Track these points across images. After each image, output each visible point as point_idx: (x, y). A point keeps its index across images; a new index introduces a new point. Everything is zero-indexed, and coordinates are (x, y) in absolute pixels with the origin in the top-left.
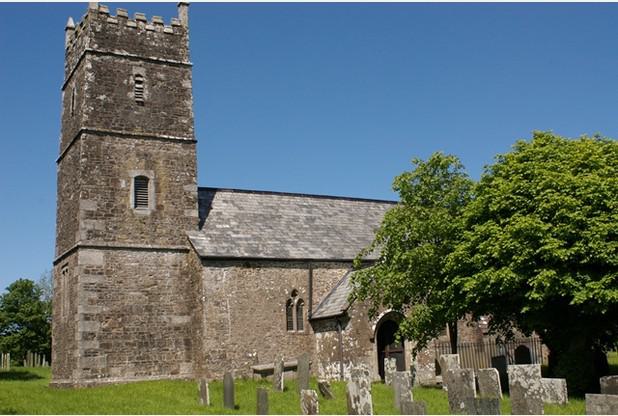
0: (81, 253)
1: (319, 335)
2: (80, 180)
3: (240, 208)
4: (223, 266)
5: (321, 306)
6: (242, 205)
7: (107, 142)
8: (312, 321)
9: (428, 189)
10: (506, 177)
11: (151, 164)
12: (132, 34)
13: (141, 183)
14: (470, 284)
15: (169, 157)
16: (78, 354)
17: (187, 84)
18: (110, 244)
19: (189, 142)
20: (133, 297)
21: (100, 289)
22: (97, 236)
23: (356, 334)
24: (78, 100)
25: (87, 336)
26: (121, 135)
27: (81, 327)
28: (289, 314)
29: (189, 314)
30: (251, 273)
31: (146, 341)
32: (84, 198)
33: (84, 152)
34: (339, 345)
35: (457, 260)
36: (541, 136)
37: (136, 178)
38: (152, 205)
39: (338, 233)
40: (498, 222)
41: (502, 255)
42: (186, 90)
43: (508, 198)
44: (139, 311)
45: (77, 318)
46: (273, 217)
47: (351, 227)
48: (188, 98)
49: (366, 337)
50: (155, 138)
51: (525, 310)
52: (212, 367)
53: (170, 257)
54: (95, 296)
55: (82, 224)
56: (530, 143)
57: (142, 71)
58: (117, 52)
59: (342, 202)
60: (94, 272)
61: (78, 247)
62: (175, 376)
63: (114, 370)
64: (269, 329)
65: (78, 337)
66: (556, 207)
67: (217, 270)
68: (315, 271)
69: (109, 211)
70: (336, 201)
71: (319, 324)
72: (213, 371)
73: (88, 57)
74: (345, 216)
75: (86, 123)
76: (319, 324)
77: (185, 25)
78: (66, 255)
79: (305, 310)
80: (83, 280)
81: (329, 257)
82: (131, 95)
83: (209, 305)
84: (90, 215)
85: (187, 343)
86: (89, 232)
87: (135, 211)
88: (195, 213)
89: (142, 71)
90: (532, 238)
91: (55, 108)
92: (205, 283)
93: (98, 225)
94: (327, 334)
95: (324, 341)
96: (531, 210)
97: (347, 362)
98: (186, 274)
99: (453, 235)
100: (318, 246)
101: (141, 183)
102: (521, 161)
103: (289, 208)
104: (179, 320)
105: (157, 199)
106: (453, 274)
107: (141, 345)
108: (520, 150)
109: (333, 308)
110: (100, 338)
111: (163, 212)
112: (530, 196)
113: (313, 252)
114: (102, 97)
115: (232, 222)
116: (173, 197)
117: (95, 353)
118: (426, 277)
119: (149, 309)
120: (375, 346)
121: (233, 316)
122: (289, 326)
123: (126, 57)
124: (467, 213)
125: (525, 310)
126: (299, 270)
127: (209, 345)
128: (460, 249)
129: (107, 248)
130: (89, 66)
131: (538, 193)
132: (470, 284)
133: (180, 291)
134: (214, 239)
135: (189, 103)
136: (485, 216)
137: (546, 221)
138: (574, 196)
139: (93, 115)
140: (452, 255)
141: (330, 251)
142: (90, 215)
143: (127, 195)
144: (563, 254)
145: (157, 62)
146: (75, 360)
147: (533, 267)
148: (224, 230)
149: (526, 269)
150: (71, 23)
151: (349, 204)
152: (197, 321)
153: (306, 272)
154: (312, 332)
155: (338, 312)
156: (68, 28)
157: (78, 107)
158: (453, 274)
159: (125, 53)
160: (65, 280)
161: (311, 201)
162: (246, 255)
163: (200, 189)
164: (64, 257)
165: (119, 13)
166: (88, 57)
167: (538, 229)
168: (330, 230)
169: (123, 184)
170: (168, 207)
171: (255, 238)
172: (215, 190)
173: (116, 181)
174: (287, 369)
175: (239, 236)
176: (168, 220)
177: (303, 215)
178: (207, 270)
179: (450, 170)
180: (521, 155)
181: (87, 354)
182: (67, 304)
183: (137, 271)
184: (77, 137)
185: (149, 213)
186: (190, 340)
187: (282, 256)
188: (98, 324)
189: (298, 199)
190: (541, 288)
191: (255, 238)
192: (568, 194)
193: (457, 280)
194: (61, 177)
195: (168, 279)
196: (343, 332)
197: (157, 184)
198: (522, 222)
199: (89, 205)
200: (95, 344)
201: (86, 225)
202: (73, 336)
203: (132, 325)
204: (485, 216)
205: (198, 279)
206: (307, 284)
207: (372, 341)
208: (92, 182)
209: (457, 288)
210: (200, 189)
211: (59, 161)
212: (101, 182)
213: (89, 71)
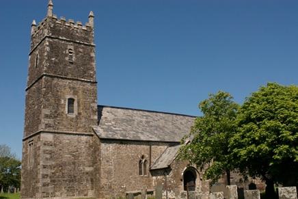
0: (42, 135)
1: (154, 178)
2: (42, 99)
3: (115, 116)
4: (111, 143)
5: (155, 163)
6: (116, 114)
7: (55, 80)
8: (151, 171)
9: (217, 108)
10: (258, 103)
11: (75, 93)
12: (67, 29)
13: (71, 101)
14: (243, 152)
15: (85, 89)
16: (40, 185)
17: (93, 55)
18: (56, 131)
19: (93, 83)
20: (67, 157)
21: (51, 153)
22: (50, 127)
23: (175, 177)
24: (40, 60)
25: (44, 176)
26: (62, 78)
27: (42, 172)
28: (140, 167)
29: (93, 166)
30: (123, 147)
31: (72, 179)
32: (44, 108)
33: (40, 86)
34: (165, 182)
35: (235, 141)
36: (272, 85)
37: (69, 99)
38: (76, 113)
39: (161, 129)
40: (256, 123)
41: (260, 138)
42: (92, 57)
43: (260, 112)
44: (69, 165)
45: (39, 167)
46: (130, 121)
47: (166, 126)
48: (93, 61)
49: (178, 178)
50: (78, 80)
51: (271, 164)
52: (105, 192)
53: (84, 138)
54: (48, 156)
55: (43, 120)
56: (267, 90)
57: (72, 47)
58: (60, 38)
59: (161, 114)
60: (48, 145)
61: (41, 132)
62: (86, 197)
63: (57, 193)
64: (131, 174)
65: (40, 176)
66: (287, 117)
67: (108, 145)
68: (152, 147)
69: (56, 115)
70: (158, 114)
71: (154, 172)
72: (106, 194)
73: (47, 39)
74: (162, 121)
75: (46, 71)
76: (154, 172)
77: (92, 27)
78: (31, 134)
79: (148, 166)
80: (42, 148)
81: (159, 140)
82: (67, 59)
83: (103, 162)
84: (47, 116)
85: (92, 180)
86: (46, 125)
87: (68, 115)
88: (96, 117)
89: (72, 47)
90: (276, 131)
91: (26, 63)
92: (102, 151)
93: (51, 121)
94: (159, 177)
95: (157, 180)
96: (272, 118)
97: (170, 191)
98: (91, 146)
99: (232, 130)
100: (153, 135)
101: (71, 101)
102: (263, 95)
103: (137, 116)
104: (88, 169)
105: (78, 110)
106: (233, 147)
107: (70, 182)
108: (263, 90)
109: (162, 164)
110: (50, 177)
111: (81, 116)
112: (271, 111)
113: (151, 138)
114: (53, 59)
115: (112, 122)
116: (86, 109)
117: (48, 185)
118: (221, 150)
119: (74, 163)
120: (183, 183)
121: (115, 167)
122: (140, 173)
123: (64, 40)
124: (238, 120)
125: (271, 164)
126: (162, 147)
127: (104, 181)
128: (237, 136)
129: (55, 133)
130: (48, 44)
131: (276, 110)
132: (243, 152)
133: (89, 155)
134: (105, 130)
135: (94, 64)
136: (248, 120)
137: (282, 123)
138: (295, 111)
139: (49, 68)
140: (232, 139)
141: (159, 137)
142: (47, 116)
143: (64, 107)
144: (291, 138)
145: (79, 43)
146: (38, 188)
147: (275, 144)
148: (109, 126)
149: (272, 145)
150: (34, 23)
151: (164, 115)
152: (97, 170)
153: (148, 147)
154: (151, 176)
155: (166, 166)
156: (33, 25)
157: (41, 63)
158: (233, 147)
159: (65, 38)
160: (31, 149)
161: (147, 113)
162: (121, 138)
163: (98, 106)
164: (31, 137)
165: (62, 19)
166: (47, 39)
167: (279, 126)
168: (157, 127)
169: (63, 102)
170: (84, 114)
171: (124, 130)
172: (103, 107)
173: (59, 100)
174: (148, 193)
175: (117, 129)
176: (83, 120)
177: (144, 120)
178: (103, 145)
179: (227, 99)
180: (263, 93)
181: (44, 185)
182: (32, 160)
183: (69, 144)
184: (41, 78)
185: (74, 116)
186: (94, 179)
187: (138, 139)
188: (50, 170)
189: (141, 112)
190: (280, 153)
191: (124, 130)
192: (292, 111)
193: (235, 150)
194: (28, 98)
195: (83, 149)
196: (167, 176)
197: (78, 102)
198: (272, 123)
199: (46, 111)
200: (48, 180)
201: (44, 121)
202: (37, 176)
203: (66, 171)
204: (248, 120)
205: (98, 149)
206: (149, 153)
207: (181, 180)
208: (48, 100)
209: (235, 154)
210: (98, 106)
211: (27, 90)
212: (52, 100)
213: (48, 46)
